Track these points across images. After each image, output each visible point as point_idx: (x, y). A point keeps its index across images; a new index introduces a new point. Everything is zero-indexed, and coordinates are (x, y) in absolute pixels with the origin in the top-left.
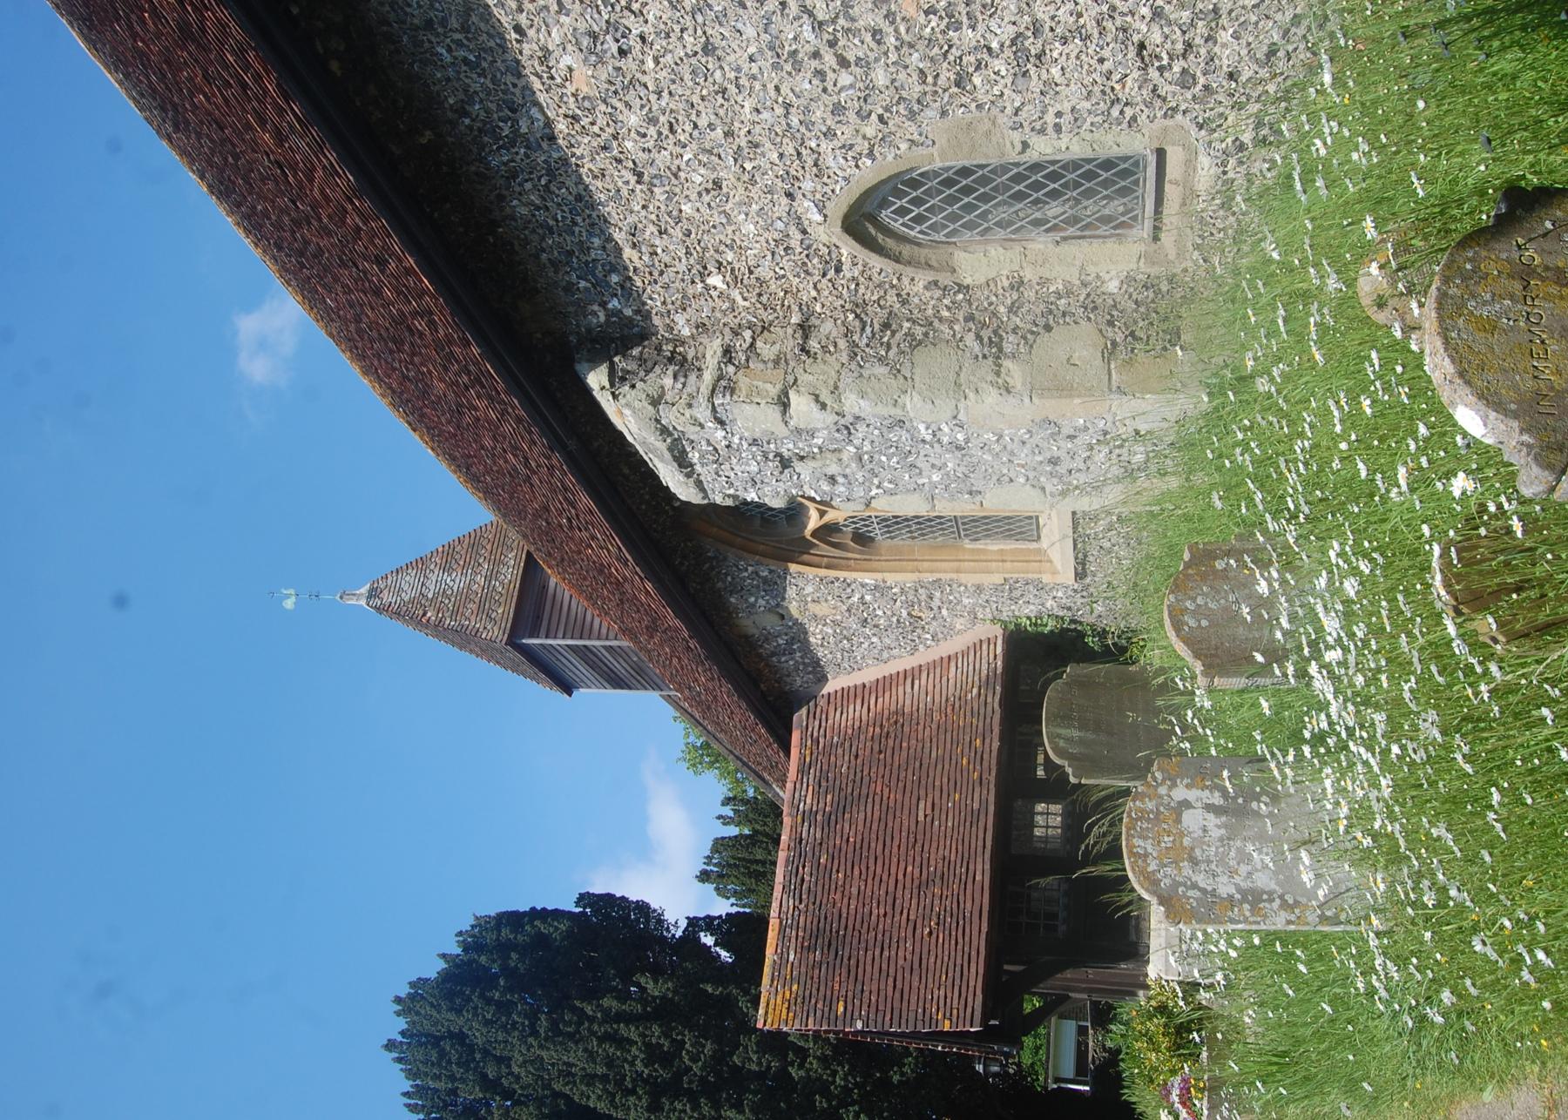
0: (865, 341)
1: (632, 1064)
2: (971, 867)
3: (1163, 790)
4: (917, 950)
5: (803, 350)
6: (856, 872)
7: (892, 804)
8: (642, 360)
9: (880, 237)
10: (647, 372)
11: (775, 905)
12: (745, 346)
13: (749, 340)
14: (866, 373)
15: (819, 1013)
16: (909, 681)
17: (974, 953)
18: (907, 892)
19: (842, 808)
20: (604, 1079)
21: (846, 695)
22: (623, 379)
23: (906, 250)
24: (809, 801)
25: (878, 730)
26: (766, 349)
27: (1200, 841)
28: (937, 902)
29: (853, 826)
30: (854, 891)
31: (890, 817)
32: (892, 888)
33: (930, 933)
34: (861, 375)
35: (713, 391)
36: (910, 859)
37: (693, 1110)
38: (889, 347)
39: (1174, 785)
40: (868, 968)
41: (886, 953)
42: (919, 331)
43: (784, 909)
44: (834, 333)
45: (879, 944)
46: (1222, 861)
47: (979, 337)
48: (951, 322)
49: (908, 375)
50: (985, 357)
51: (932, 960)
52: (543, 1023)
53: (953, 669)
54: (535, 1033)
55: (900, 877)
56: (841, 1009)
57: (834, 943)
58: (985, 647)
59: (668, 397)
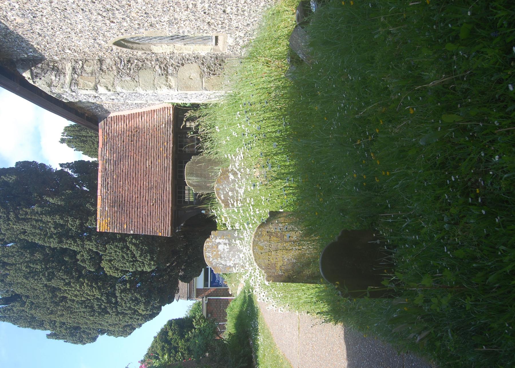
0: (122, 67)
1: (50, 229)
2: (165, 185)
3: (213, 240)
4: (149, 210)
5: (101, 69)
6: (127, 182)
7: (137, 160)
8: (42, 69)
9: (126, 44)
10: (45, 74)
11: (99, 191)
12: (80, 67)
13: (81, 65)
14: (123, 79)
15: (118, 228)
16: (140, 117)
17: (167, 213)
18: (144, 190)
19: (120, 159)
20: (40, 234)
21: (118, 118)
22: (36, 76)
23: (135, 46)
24: (107, 155)
25: (130, 133)
26: (88, 69)
27: (223, 252)
28: (154, 195)
29: (125, 166)
30: (127, 188)
31: (137, 164)
32: (139, 189)
33: (153, 205)
34: (122, 80)
35: (71, 84)
36: (145, 180)
37: (74, 243)
38: (130, 70)
39: (216, 239)
40: (133, 214)
41: (139, 210)
42: (140, 64)
43: (102, 192)
44: (111, 63)
45: (136, 207)
46: (228, 257)
47: (160, 67)
48: (151, 61)
49: (138, 81)
50: (162, 75)
51: (154, 213)
52: (12, 215)
53: (156, 115)
54: (9, 219)
55: (142, 185)
56: (125, 227)
57: (121, 205)
58: (166, 110)
59: (54, 84)
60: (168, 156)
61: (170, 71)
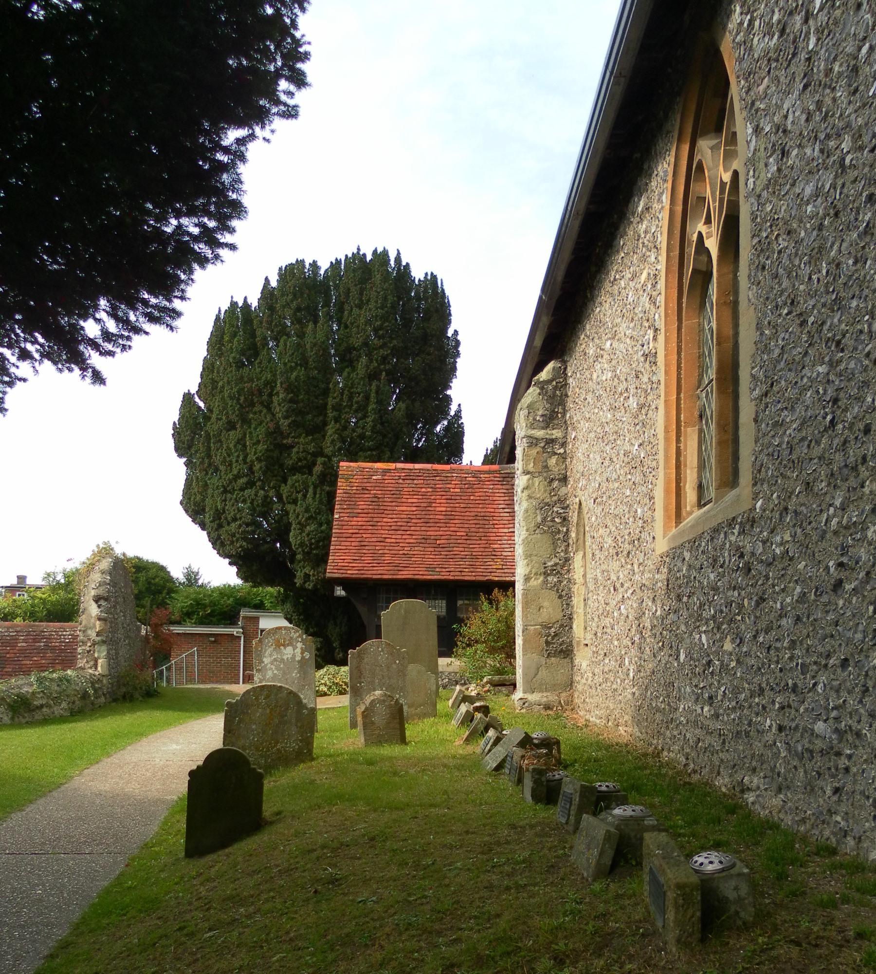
13: (559, 452)
17: (362, 572)
26: (553, 461)
32: (403, 528)
60: (452, 574)
61: (550, 579)
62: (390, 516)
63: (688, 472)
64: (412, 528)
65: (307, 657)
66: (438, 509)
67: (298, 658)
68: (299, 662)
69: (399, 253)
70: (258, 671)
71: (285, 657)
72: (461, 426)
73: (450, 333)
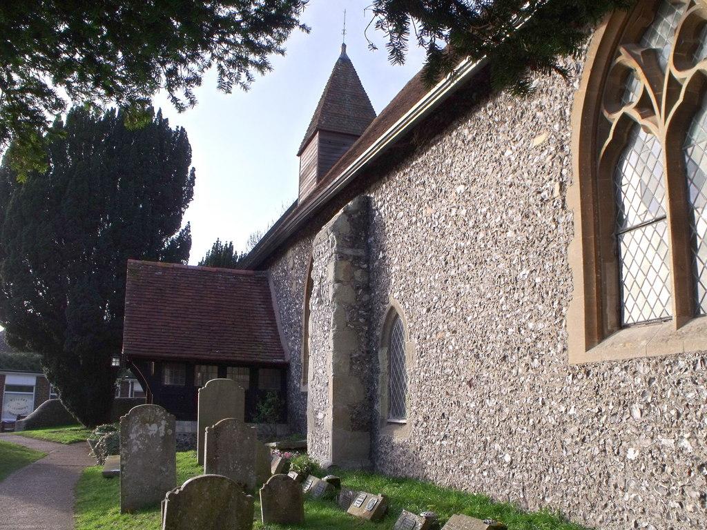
17: (152, 350)
62: (171, 305)
63: (608, 297)
64: (190, 316)
65: (170, 434)
66: (209, 302)
67: (162, 434)
68: (163, 438)
69: (160, 110)
70: (125, 446)
71: (150, 434)
72: (189, 237)
73: (190, 168)
